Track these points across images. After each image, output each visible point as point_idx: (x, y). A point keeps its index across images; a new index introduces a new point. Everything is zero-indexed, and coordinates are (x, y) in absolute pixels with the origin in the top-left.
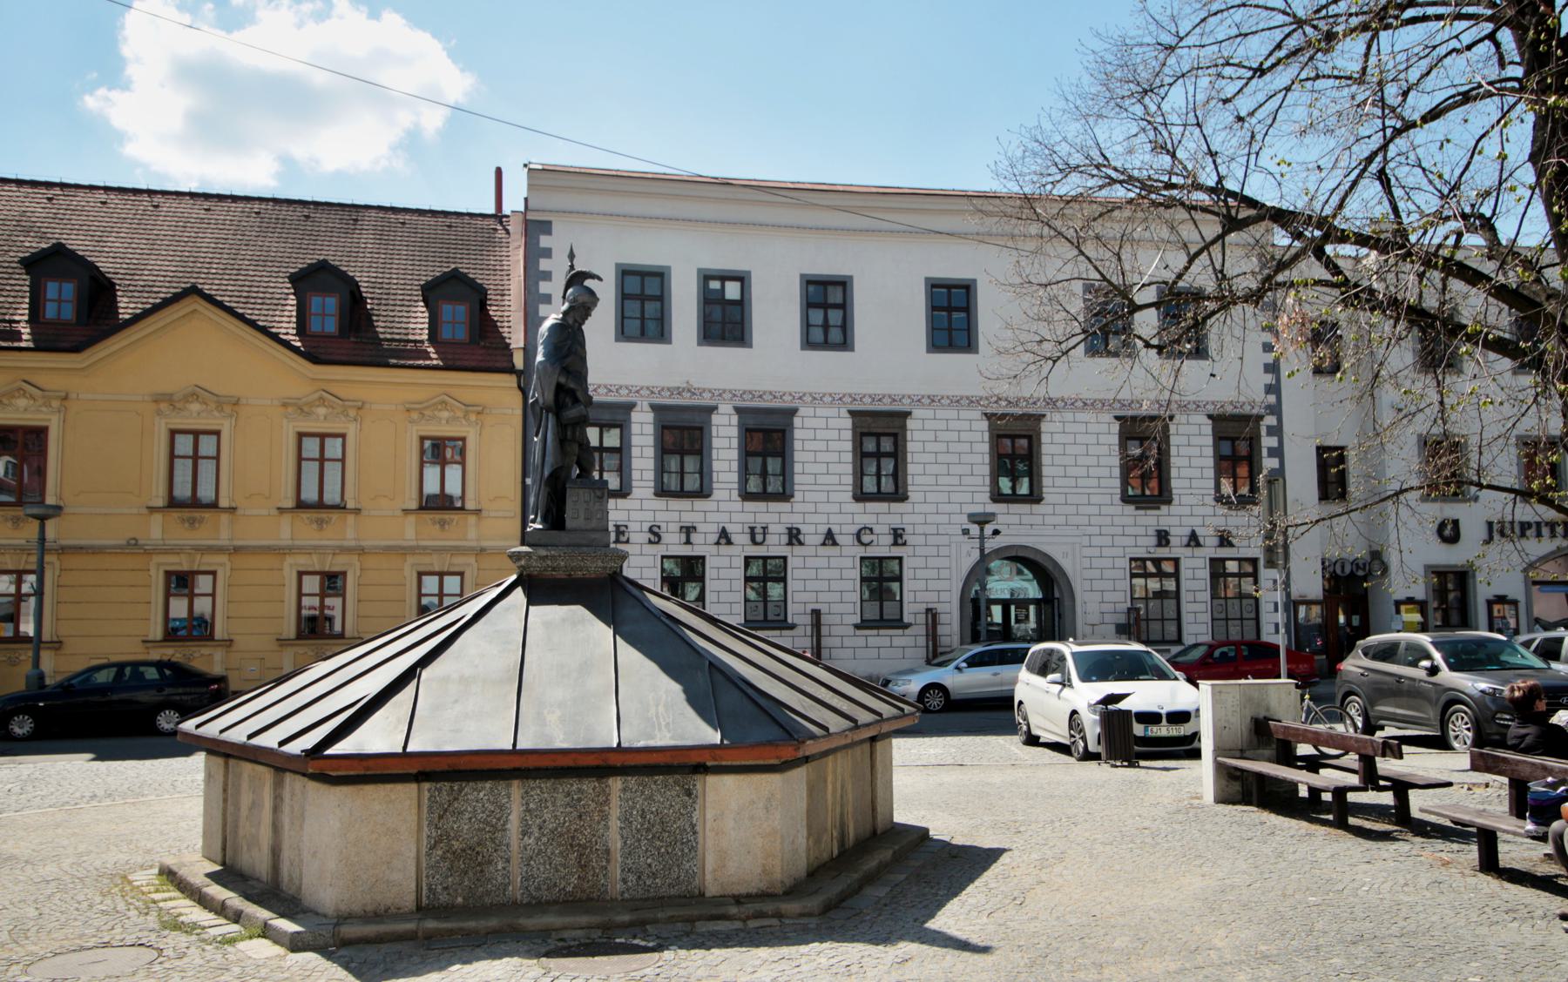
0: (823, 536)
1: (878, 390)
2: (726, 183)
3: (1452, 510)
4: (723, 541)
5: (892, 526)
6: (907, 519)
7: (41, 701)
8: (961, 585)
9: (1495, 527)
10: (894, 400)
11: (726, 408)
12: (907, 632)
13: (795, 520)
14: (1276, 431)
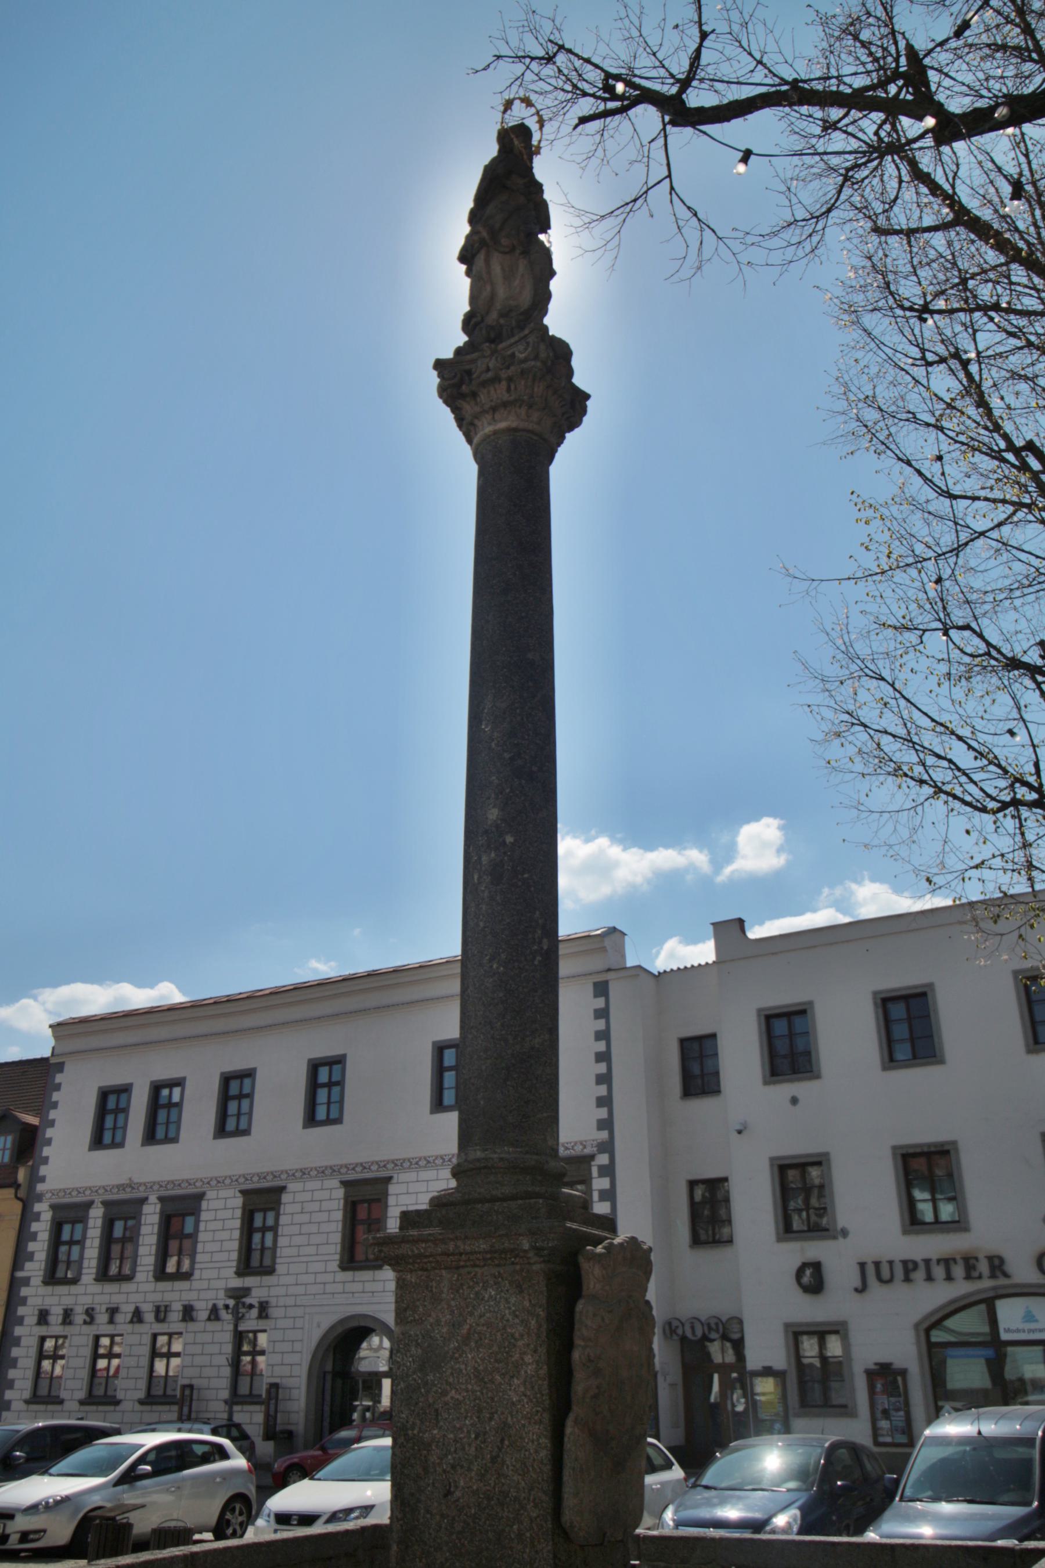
0: (208, 1312)
1: (178, 1176)
2: (230, 1000)
3: (814, 1250)
4: (187, 1318)
5: (156, 1304)
6: (274, 1291)
7: (840, 1480)
8: (310, 1357)
9: (871, 1270)
10: (275, 1177)
11: (153, 1199)
12: (118, 1408)
13: (189, 1297)
14: (608, 1171)
